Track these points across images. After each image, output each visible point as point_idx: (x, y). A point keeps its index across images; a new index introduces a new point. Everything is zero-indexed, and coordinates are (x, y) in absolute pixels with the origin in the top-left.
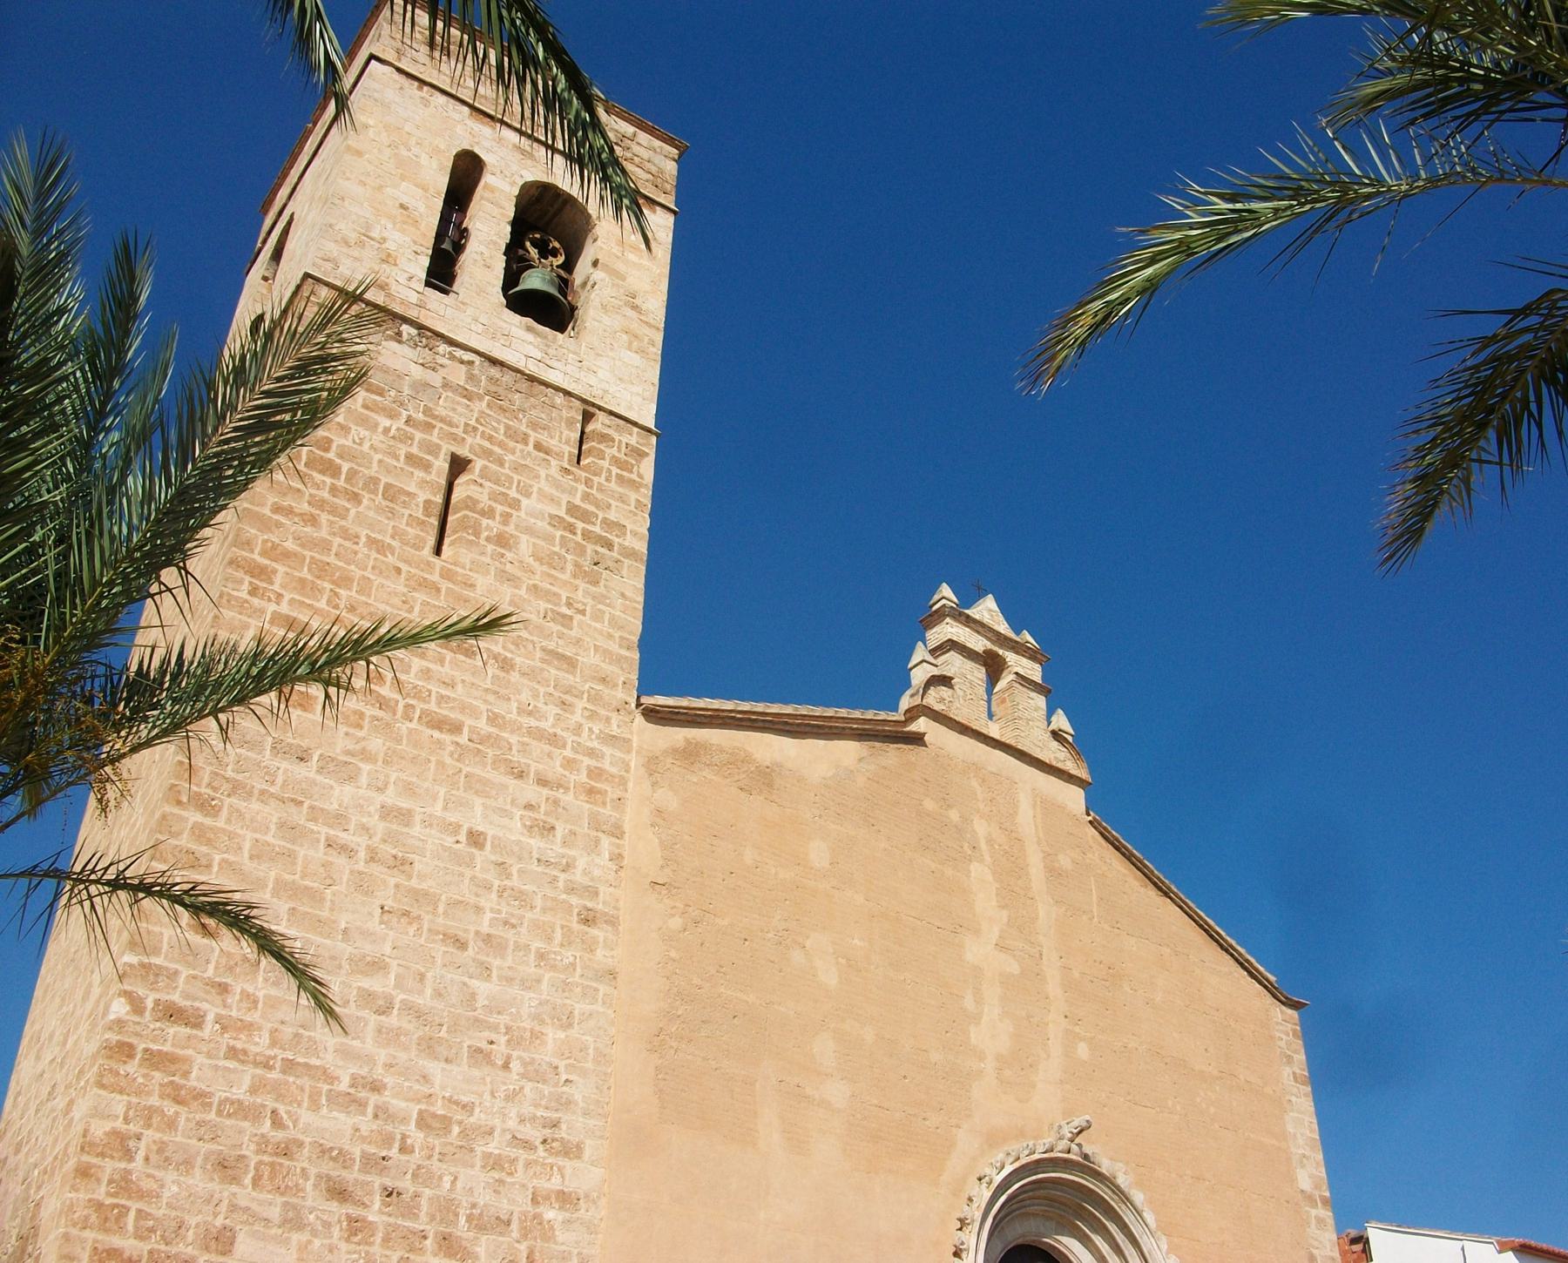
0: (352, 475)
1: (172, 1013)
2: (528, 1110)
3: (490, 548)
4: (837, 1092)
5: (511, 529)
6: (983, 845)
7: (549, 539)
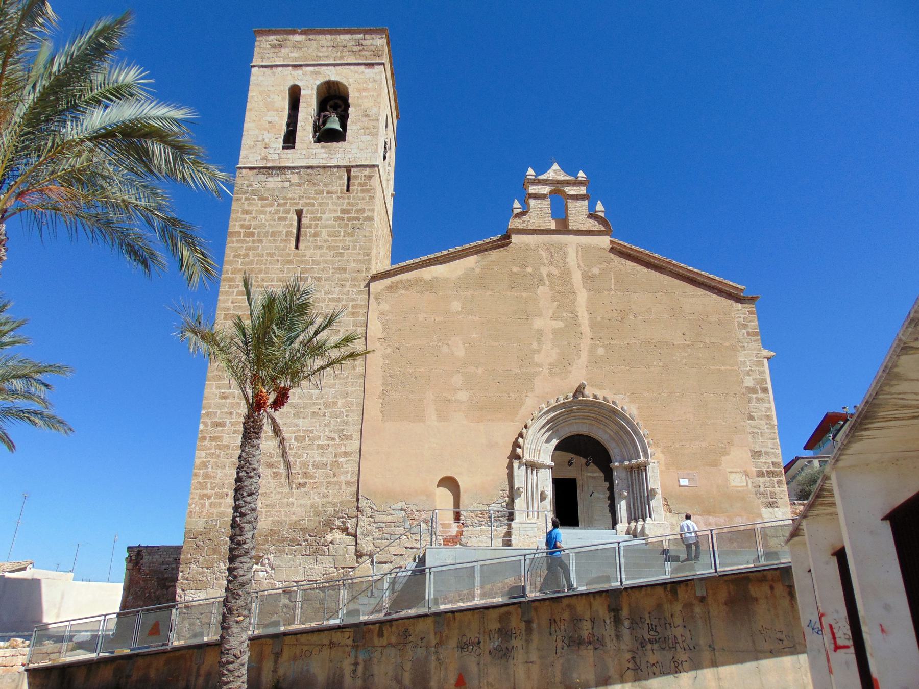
0: (259, 233)
1: (217, 424)
2: (332, 427)
3: (311, 239)
4: (463, 396)
5: (319, 229)
6: (545, 277)
7: (334, 226)
